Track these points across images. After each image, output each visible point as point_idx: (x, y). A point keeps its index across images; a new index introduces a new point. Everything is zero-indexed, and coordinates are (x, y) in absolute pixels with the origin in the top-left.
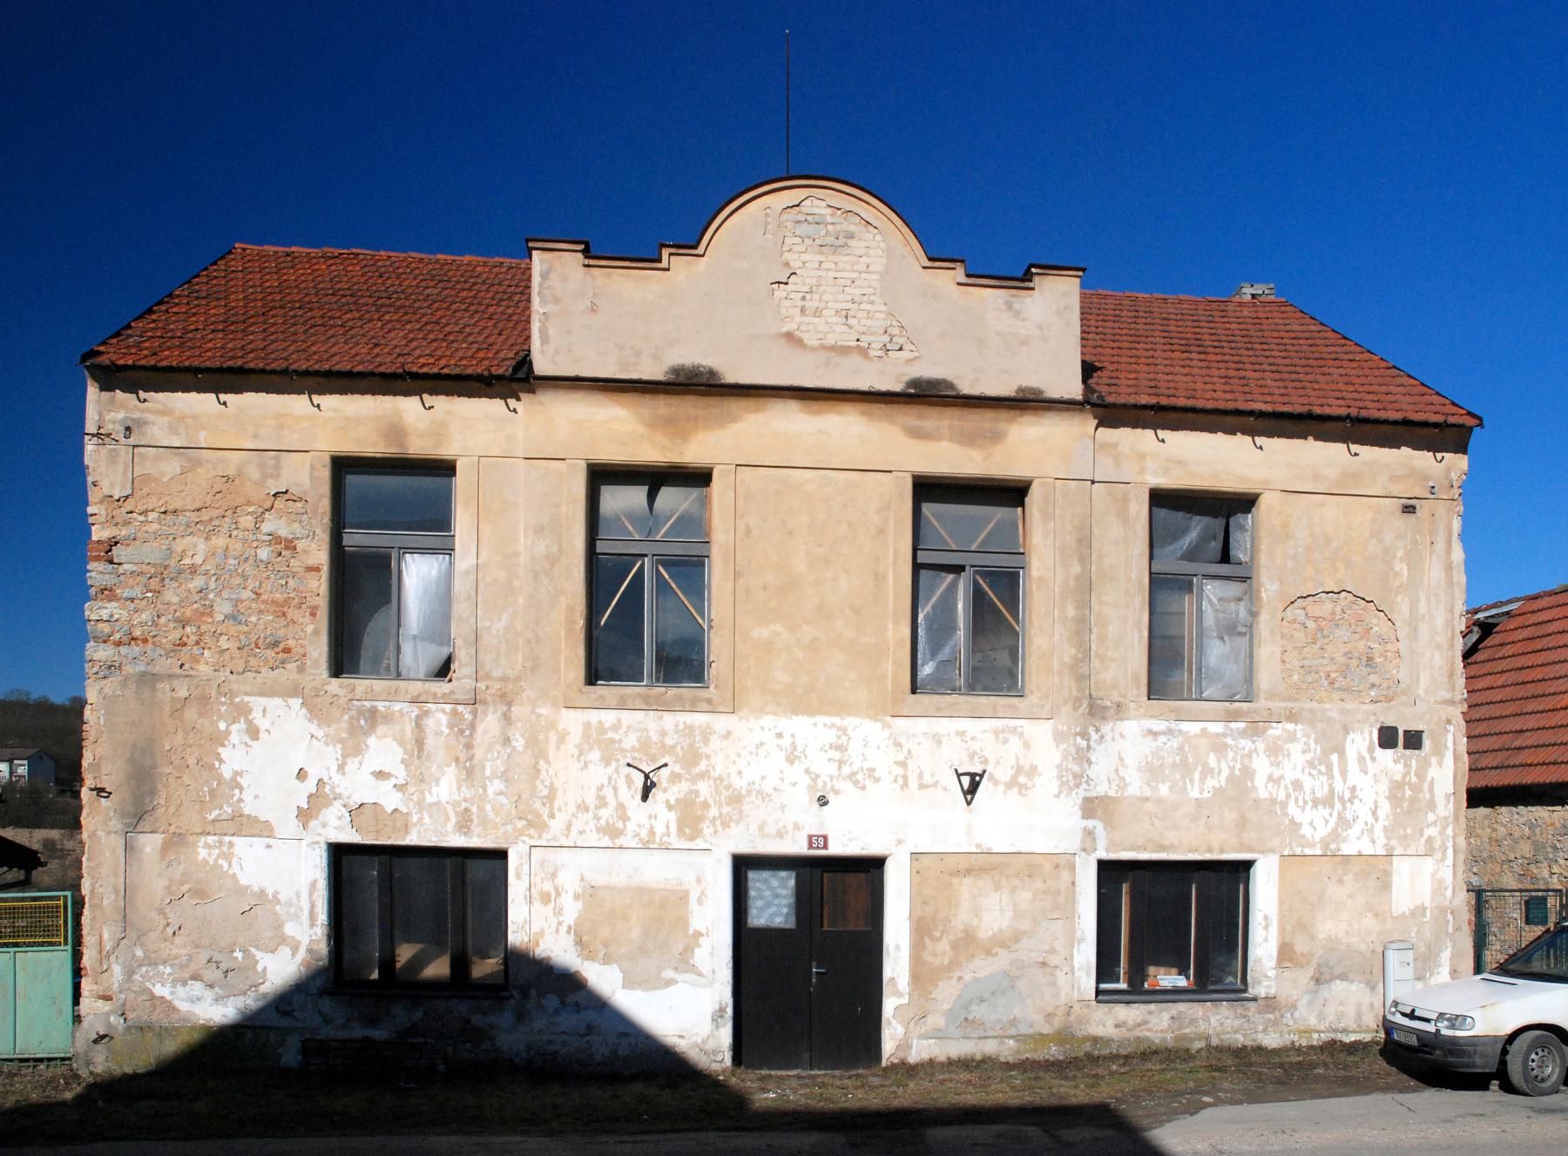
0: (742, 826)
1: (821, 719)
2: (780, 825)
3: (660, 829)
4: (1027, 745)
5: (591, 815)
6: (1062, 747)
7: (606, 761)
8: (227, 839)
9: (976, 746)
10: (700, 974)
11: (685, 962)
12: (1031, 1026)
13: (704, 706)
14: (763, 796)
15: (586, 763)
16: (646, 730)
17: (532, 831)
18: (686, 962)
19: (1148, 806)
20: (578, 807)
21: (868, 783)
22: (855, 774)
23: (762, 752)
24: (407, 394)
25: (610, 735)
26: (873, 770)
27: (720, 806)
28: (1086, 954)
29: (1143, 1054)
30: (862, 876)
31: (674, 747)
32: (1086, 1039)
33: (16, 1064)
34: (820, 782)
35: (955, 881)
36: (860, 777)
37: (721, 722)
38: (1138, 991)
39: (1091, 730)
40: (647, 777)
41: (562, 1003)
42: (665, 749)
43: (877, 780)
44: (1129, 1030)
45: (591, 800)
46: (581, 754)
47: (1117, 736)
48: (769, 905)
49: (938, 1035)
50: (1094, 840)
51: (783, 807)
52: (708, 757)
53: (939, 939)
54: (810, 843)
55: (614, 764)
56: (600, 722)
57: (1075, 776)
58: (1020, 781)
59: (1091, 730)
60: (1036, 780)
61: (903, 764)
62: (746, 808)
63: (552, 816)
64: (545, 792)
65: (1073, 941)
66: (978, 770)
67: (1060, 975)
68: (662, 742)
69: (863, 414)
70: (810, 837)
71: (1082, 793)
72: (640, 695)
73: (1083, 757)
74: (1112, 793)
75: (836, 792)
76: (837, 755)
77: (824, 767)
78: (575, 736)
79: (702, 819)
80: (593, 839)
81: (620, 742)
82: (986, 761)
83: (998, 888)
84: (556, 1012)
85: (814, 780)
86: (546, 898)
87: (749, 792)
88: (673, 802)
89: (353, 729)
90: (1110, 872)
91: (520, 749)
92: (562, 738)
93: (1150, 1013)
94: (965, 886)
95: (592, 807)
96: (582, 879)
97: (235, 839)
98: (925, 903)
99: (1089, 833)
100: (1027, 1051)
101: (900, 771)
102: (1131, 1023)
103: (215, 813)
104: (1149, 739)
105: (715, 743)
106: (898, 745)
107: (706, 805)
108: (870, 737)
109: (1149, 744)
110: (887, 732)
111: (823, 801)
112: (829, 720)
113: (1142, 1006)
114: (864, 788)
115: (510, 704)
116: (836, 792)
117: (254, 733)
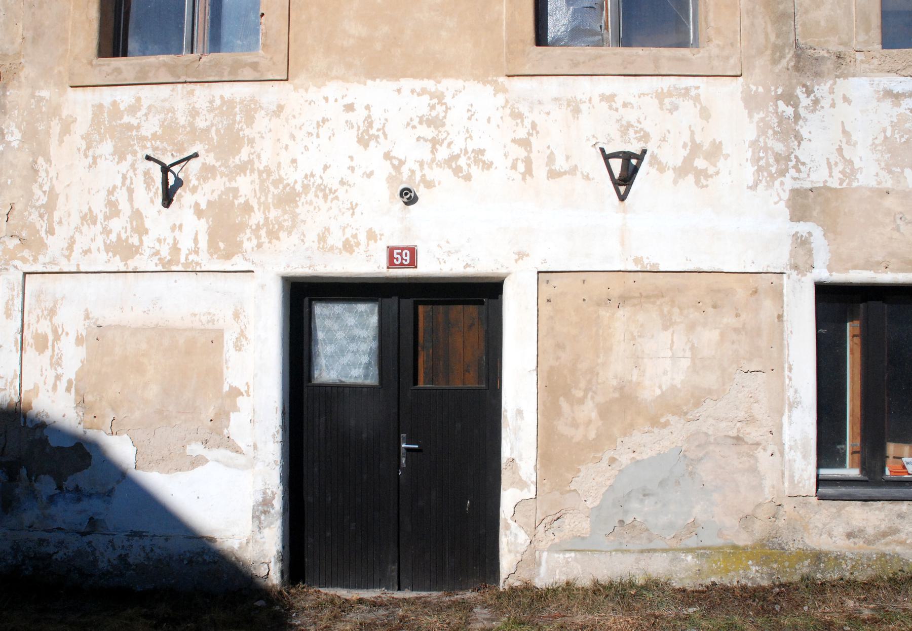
0: (295, 238)
1: (407, 84)
2: (349, 233)
3: (186, 244)
4: (705, 113)
5: (99, 227)
6: (757, 117)
7: (120, 154)
9: (631, 116)
10: (238, 451)
11: (217, 435)
12: (720, 533)
13: (248, 73)
14: (325, 192)
15: (95, 159)
16: (172, 110)
17: (26, 253)
18: (220, 433)
19: (890, 202)
20: (84, 218)
21: (475, 171)
22: (456, 157)
23: (324, 131)
25: (126, 119)
26: (482, 152)
27: (267, 208)
28: (802, 424)
29: (893, 580)
30: (472, 310)
31: (207, 130)
32: (802, 555)
34: (405, 170)
35: (604, 313)
36: (462, 162)
37: (270, 94)
38: (876, 482)
39: (800, 92)
40: (165, 170)
41: (60, 487)
42: (195, 134)
43: (488, 166)
44: (869, 542)
45: (99, 207)
46: (88, 148)
47: (839, 102)
48: (342, 351)
49: (579, 546)
50: (810, 252)
51: (353, 208)
52: (251, 141)
53: (582, 401)
54: (391, 258)
55: (129, 157)
56: (114, 104)
57: (778, 158)
58: (699, 163)
59: (800, 92)
60: (721, 163)
61: (525, 143)
62: (301, 210)
63: (51, 231)
64: (44, 200)
65: (781, 405)
66: (635, 149)
67: (762, 456)
68: (191, 124)
70: (391, 250)
71: (789, 183)
72: (165, 64)
73: (789, 130)
74: (834, 183)
75: (429, 185)
76: (428, 132)
77: (411, 150)
78: (81, 127)
79: (241, 227)
80: (100, 261)
81: (138, 127)
82: (646, 137)
83: (668, 324)
84: (51, 499)
85: (397, 168)
86: (42, 344)
87: (306, 188)
88: (203, 206)
90: (834, 301)
91: (15, 144)
92: (66, 129)
93: (901, 516)
94: (620, 321)
95: (100, 217)
96: (87, 317)
98: (560, 346)
99: (802, 243)
100: (714, 573)
101: (521, 153)
102: (870, 531)
104: (888, 103)
105: (262, 122)
106: (517, 116)
107: (247, 208)
108: (477, 107)
109: (888, 112)
110: (501, 98)
111: (409, 197)
112: (418, 84)
113: (888, 505)
114: (468, 178)
116: (429, 185)
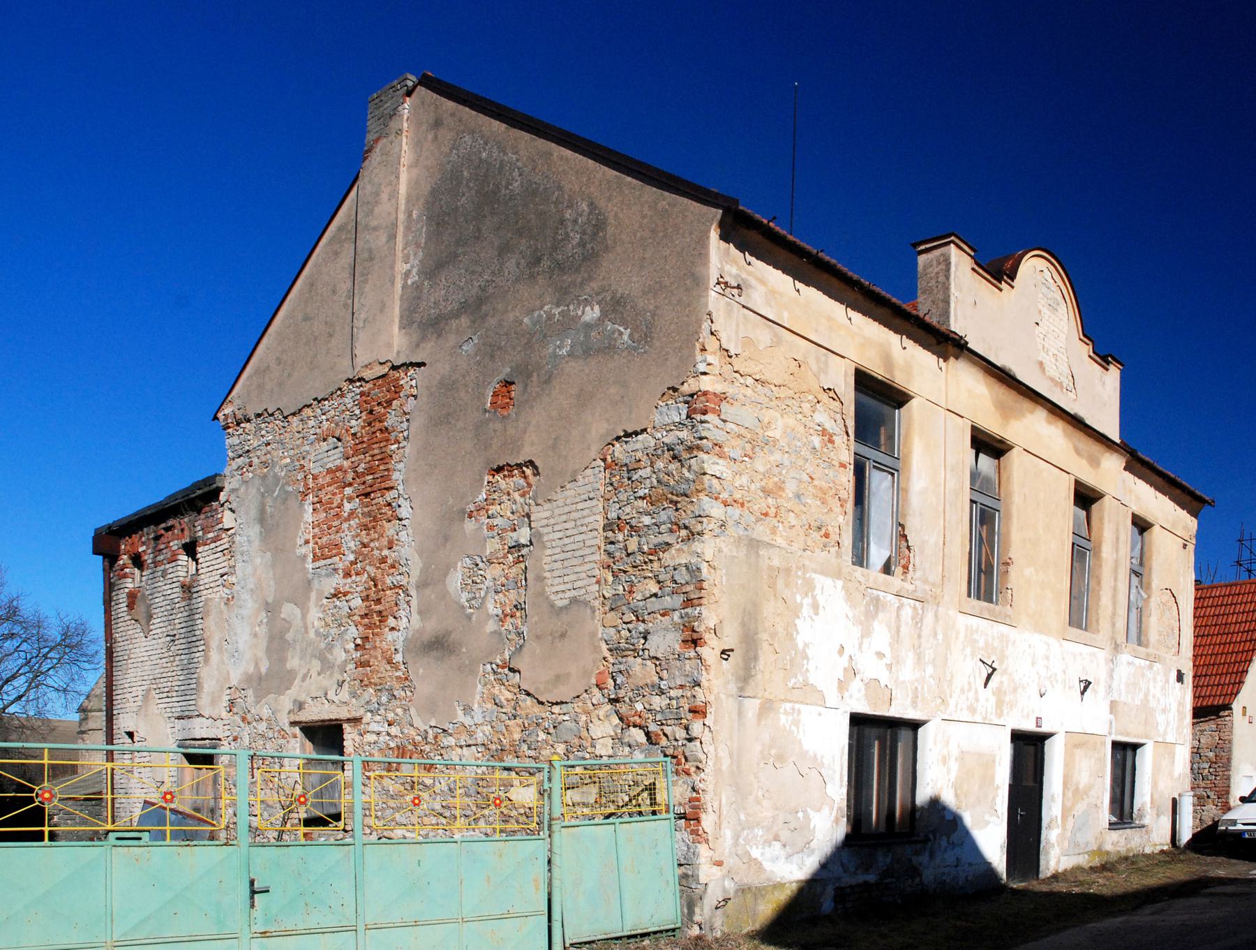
8: (797, 706)
24: (896, 332)
33: (625, 940)
69: (1066, 434)
89: (867, 612)
97: (802, 707)
103: (793, 680)
115: (938, 605)
117: (816, 607)
